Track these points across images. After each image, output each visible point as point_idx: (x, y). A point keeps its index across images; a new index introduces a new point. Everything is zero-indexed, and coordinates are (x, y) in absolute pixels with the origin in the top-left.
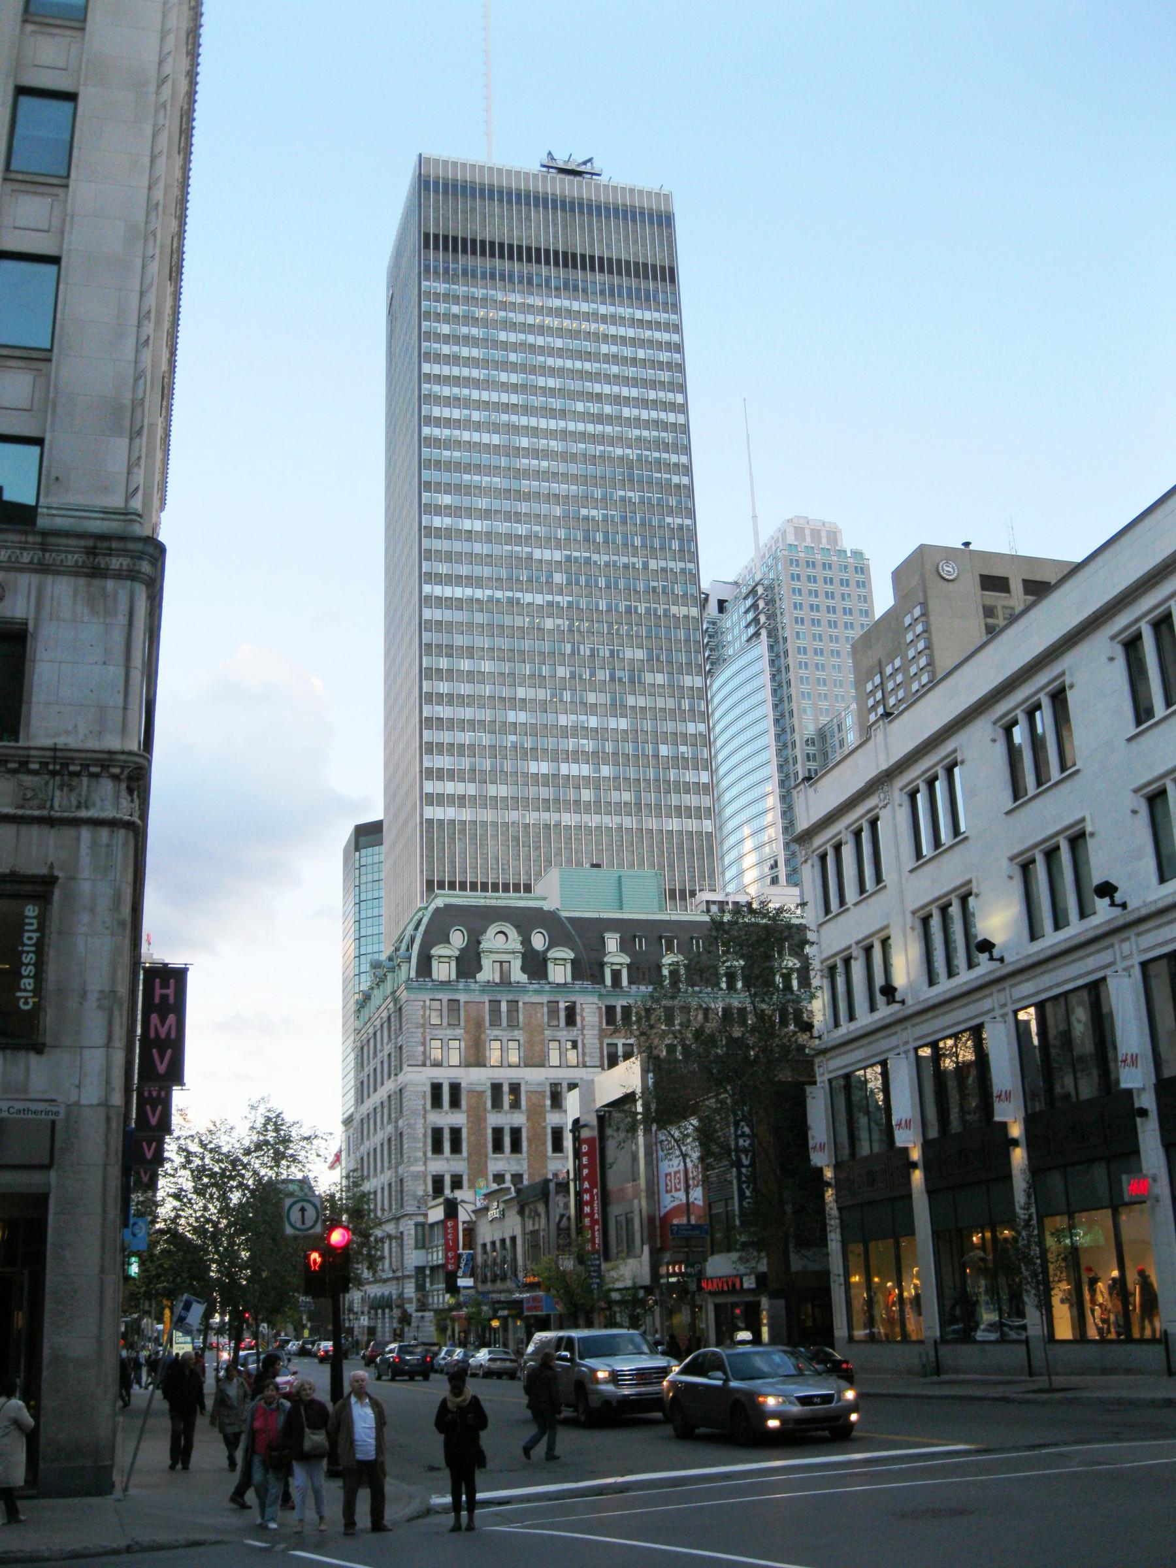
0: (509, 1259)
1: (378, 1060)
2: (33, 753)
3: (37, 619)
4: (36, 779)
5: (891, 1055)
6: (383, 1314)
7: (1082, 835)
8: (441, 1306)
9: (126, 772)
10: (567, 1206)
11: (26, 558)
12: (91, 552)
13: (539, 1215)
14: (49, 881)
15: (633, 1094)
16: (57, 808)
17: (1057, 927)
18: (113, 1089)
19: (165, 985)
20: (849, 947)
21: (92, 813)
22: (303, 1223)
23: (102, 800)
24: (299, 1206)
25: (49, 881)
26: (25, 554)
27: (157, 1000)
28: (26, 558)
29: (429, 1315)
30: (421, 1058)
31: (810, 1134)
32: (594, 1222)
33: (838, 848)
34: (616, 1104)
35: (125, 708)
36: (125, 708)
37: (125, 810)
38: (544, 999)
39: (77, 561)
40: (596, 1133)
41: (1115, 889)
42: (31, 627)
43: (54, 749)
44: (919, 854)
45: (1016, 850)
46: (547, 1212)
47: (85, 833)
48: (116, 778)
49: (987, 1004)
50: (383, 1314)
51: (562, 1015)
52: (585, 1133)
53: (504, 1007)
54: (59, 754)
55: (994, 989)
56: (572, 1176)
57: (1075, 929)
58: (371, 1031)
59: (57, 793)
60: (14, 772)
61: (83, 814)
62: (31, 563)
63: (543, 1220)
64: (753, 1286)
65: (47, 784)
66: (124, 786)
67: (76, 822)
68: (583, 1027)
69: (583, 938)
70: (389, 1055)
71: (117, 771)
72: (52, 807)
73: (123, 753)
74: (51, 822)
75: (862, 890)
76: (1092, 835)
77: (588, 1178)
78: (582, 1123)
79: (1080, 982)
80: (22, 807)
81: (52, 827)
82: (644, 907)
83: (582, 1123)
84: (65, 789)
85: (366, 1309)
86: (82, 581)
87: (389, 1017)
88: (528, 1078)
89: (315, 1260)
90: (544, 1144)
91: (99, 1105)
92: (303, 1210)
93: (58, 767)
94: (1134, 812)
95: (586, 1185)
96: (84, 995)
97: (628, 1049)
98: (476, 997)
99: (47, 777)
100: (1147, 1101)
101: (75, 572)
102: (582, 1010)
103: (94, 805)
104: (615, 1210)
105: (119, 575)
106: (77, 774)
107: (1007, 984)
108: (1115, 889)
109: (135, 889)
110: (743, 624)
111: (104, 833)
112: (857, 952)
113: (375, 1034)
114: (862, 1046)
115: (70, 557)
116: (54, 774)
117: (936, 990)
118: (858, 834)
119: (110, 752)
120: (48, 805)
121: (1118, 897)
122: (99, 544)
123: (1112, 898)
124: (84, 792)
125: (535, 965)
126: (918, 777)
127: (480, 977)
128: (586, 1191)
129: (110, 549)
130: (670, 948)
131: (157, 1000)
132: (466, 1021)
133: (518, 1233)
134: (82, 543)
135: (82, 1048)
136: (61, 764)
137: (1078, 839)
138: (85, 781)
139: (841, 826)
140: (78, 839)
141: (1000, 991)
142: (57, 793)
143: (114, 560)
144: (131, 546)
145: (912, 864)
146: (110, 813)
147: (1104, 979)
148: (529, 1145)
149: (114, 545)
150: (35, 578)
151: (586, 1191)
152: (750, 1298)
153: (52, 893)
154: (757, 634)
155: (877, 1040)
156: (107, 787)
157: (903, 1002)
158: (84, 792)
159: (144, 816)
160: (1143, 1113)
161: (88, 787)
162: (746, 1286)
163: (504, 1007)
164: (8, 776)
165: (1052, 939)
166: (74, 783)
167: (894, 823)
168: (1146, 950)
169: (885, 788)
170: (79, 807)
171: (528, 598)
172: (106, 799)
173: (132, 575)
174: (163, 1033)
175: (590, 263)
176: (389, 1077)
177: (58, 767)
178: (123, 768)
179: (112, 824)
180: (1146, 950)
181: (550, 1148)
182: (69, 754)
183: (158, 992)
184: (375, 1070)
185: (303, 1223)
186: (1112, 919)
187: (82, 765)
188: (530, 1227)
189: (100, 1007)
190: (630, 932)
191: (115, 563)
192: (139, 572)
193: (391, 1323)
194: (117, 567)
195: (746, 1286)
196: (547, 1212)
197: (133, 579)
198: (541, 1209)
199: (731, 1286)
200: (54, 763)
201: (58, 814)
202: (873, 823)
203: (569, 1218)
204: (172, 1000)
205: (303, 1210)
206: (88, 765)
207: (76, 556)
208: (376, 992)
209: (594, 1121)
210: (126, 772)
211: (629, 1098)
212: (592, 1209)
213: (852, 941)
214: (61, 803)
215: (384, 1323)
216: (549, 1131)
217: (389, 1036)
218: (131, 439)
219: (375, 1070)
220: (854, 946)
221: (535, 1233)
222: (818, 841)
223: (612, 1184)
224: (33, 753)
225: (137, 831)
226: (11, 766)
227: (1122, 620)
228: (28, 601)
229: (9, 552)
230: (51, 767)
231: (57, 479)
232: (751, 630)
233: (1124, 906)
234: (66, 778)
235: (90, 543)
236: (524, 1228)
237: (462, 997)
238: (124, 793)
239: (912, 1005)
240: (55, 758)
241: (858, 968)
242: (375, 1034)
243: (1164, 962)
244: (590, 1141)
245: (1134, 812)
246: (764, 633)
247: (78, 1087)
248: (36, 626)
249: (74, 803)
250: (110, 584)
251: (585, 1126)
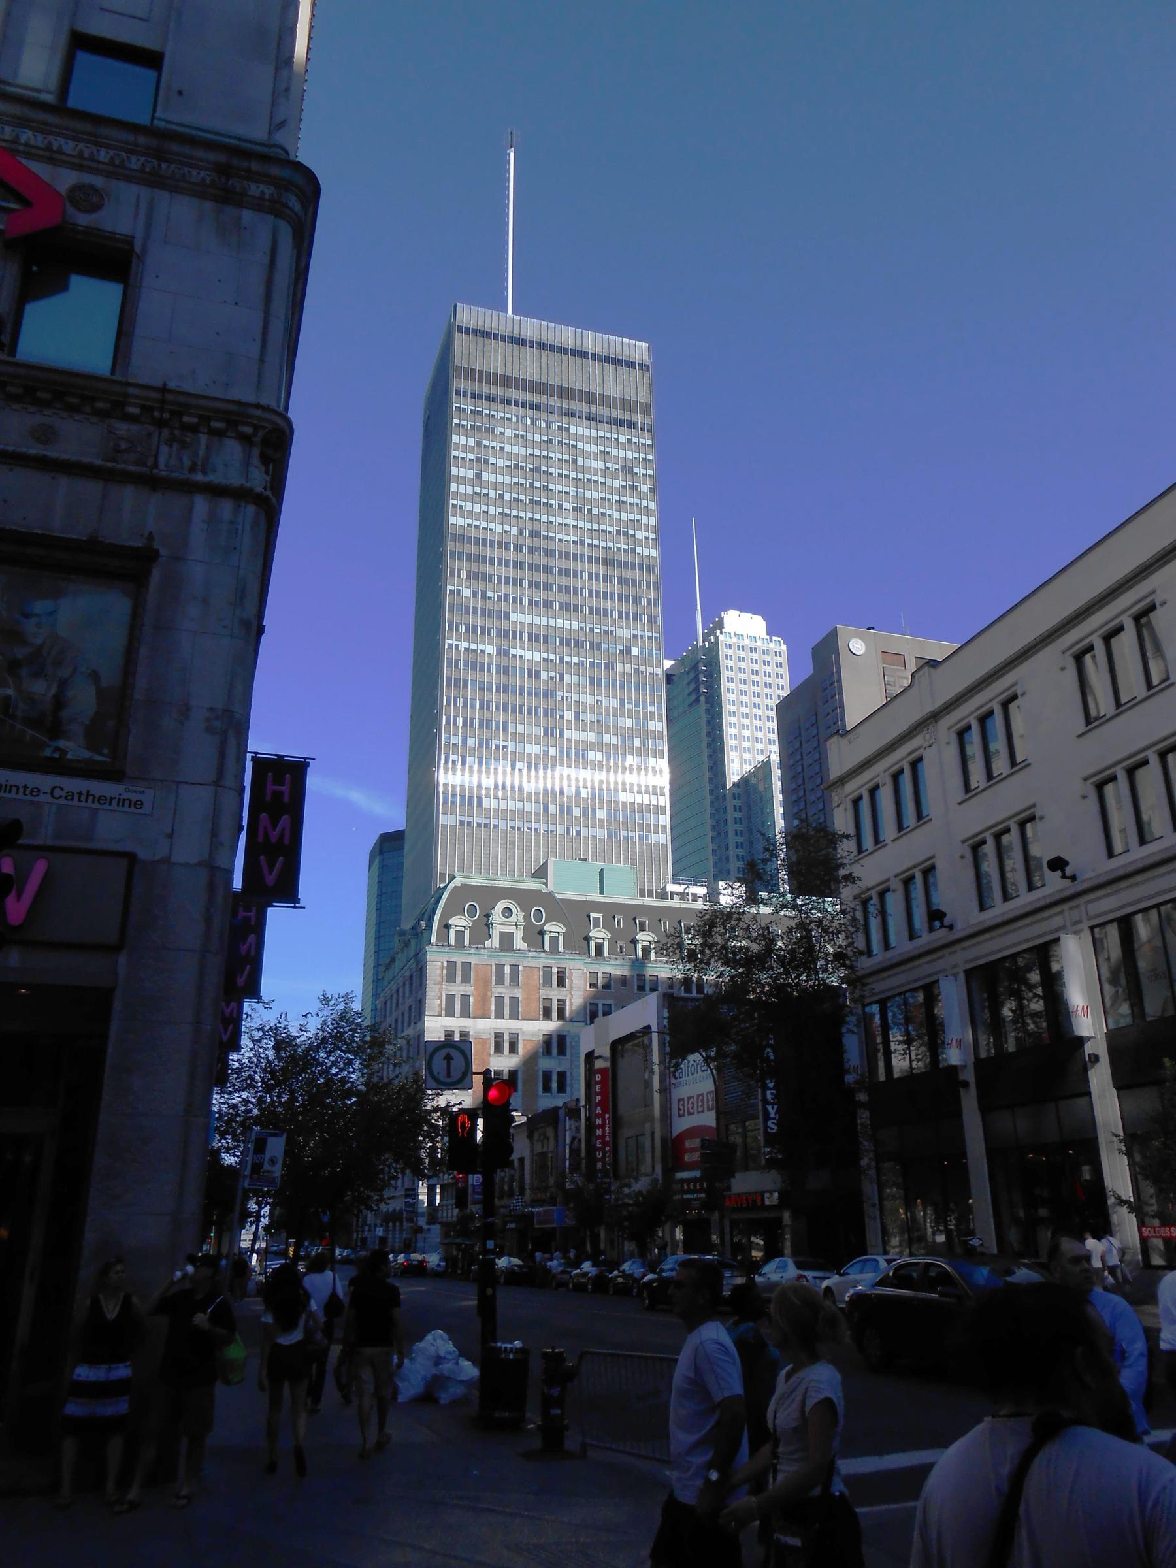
0: (517, 1176)
1: (394, 1015)
2: (131, 390)
3: (147, 237)
4: (135, 428)
5: (940, 976)
6: (394, 1227)
7: (932, 868)
8: (449, 1220)
9: (261, 433)
10: (578, 1129)
11: (135, 163)
12: (224, 170)
13: (548, 1139)
14: (145, 557)
15: (649, 1027)
16: (162, 466)
17: (1006, 897)
18: (222, 844)
19: (279, 780)
20: (888, 880)
21: (214, 478)
22: (449, 1075)
23: (226, 465)
24: (443, 1052)
25: (145, 557)
26: (134, 159)
27: (268, 797)
28: (135, 163)
29: (436, 1228)
30: (437, 1009)
31: (846, 1056)
32: (605, 1143)
33: (873, 791)
34: (631, 1037)
35: (262, 360)
36: (262, 360)
37: (258, 480)
38: (541, 964)
39: (203, 179)
40: (607, 1064)
41: (1066, 863)
42: (138, 247)
43: (164, 389)
44: (967, 788)
45: (1091, 771)
46: (556, 1136)
47: (201, 505)
48: (245, 439)
49: (1057, 921)
50: (394, 1227)
51: (555, 978)
52: (599, 1064)
53: (507, 969)
54: (169, 397)
55: (1065, 907)
56: (582, 1103)
57: (1025, 900)
58: (394, 988)
59: (164, 449)
60: (104, 415)
61: (199, 477)
62: (142, 170)
63: (552, 1141)
64: (776, 1202)
65: (149, 435)
66: (256, 452)
67: (189, 488)
68: (571, 988)
69: (576, 915)
70: (410, 1007)
71: (248, 430)
72: (156, 465)
73: (258, 406)
74: (152, 483)
75: (900, 827)
76: (1042, 818)
77: (600, 1104)
78: (596, 1054)
79: (917, 984)
80: (114, 460)
81: (154, 489)
82: (622, 893)
83: (596, 1054)
84: (175, 445)
85: (379, 1222)
86: (208, 205)
87: (411, 977)
88: (524, 1028)
89: (463, 1124)
90: (536, 1084)
91: (200, 864)
92: (448, 1058)
93: (166, 416)
94: (1084, 797)
95: (599, 1110)
96: (186, 710)
97: (607, 1009)
98: (485, 959)
99: (151, 428)
100: (969, 1076)
101: (200, 192)
102: (571, 974)
103: (214, 471)
104: (626, 1133)
105: (259, 205)
106: (194, 429)
107: (1081, 901)
108: (1066, 863)
109: (263, 574)
110: (687, 692)
111: (226, 507)
112: (897, 885)
113: (398, 991)
114: (902, 972)
115: (194, 172)
116: (160, 424)
117: (918, 942)
118: (896, 776)
119: (240, 403)
120: (150, 462)
121: (1069, 871)
122: (235, 162)
123: (1063, 871)
124: (202, 453)
125: (536, 936)
126: (1123, 612)
127: (488, 944)
128: (598, 1116)
129: (249, 171)
130: (642, 929)
131: (268, 797)
132: (476, 981)
133: (527, 1154)
134: (212, 156)
135: (178, 783)
136: (172, 412)
137: (929, 871)
138: (203, 439)
139: (880, 772)
140: (190, 510)
141: (1071, 908)
142: (164, 449)
143: (253, 187)
144: (275, 171)
145: (961, 796)
146: (235, 479)
147: (1057, 940)
148: (524, 1085)
149: (255, 166)
150: (145, 192)
151: (598, 1116)
152: (772, 1214)
153: (149, 573)
154: (697, 700)
155: (919, 965)
156: (232, 450)
157: (951, 927)
158: (202, 453)
159: (278, 484)
160: (966, 1084)
161: (208, 448)
162: (767, 1202)
163: (507, 969)
164: (95, 420)
165: (1000, 910)
166: (188, 440)
167: (940, 761)
168: (1097, 916)
169: (931, 728)
170: (192, 469)
171: (616, 515)
172: (231, 463)
173: (275, 208)
174: (274, 835)
175: (587, 397)
176: (409, 1025)
177: (166, 416)
178: (256, 428)
179: (240, 495)
180: (1097, 916)
181: (541, 1089)
182: (182, 399)
183: (270, 787)
184: (396, 1020)
185: (449, 1075)
186: (1062, 890)
187: (200, 417)
188: (538, 1149)
189: (210, 730)
190: (611, 911)
191: (254, 189)
192: (286, 205)
193: (401, 1233)
194: (257, 194)
195: (767, 1202)
196: (556, 1136)
197: (278, 214)
198: (550, 1132)
199: (753, 1201)
200: (162, 410)
201: (164, 473)
202: (915, 764)
203: (580, 1141)
204: (286, 799)
205: (448, 1058)
206: (209, 419)
207: (203, 173)
208: (399, 956)
209: (606, 1052)
210: (261, 433)
211: (647, 1030)
212: (604, 1132)
213: (891, 874)
214: (167, 460)
215: (394, 1234)
216: (541, 1074)
217: (411, 991)
218: (277, 69)
219: (396, 1020)
220: (893, 879)
221: (544, 1155)
222: (851, 787)
223: (623, 1108)
224: (131, 390)
225: (268, 507)
226: (100, 405)
227: (1073, 636)
228: (136, 216)
229: (112, 152)
230: (156, 414)
231: (180, 93)
232: (693, 697)
233: (1073, 878)
234: (177, 432)
235: (221, 158)
236: (532, 1151)
237: (473, 960)
238: (256, 461)
239: (960, 931)
240: (163, 401)
241: (895, 902)
242: (398, 991)
243: (1115, 925)
244: (603, 1071)
245: (1084, 797)
246: (702, 699)
247: (170, 836)
248: (144, 248)
249: (187, 462)
250: (247, 215)
251: (599, 1057)
